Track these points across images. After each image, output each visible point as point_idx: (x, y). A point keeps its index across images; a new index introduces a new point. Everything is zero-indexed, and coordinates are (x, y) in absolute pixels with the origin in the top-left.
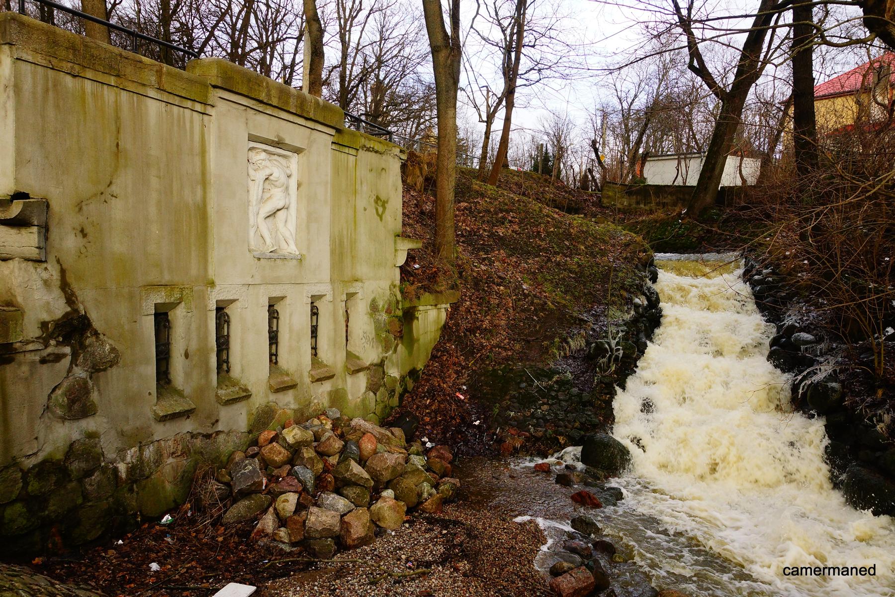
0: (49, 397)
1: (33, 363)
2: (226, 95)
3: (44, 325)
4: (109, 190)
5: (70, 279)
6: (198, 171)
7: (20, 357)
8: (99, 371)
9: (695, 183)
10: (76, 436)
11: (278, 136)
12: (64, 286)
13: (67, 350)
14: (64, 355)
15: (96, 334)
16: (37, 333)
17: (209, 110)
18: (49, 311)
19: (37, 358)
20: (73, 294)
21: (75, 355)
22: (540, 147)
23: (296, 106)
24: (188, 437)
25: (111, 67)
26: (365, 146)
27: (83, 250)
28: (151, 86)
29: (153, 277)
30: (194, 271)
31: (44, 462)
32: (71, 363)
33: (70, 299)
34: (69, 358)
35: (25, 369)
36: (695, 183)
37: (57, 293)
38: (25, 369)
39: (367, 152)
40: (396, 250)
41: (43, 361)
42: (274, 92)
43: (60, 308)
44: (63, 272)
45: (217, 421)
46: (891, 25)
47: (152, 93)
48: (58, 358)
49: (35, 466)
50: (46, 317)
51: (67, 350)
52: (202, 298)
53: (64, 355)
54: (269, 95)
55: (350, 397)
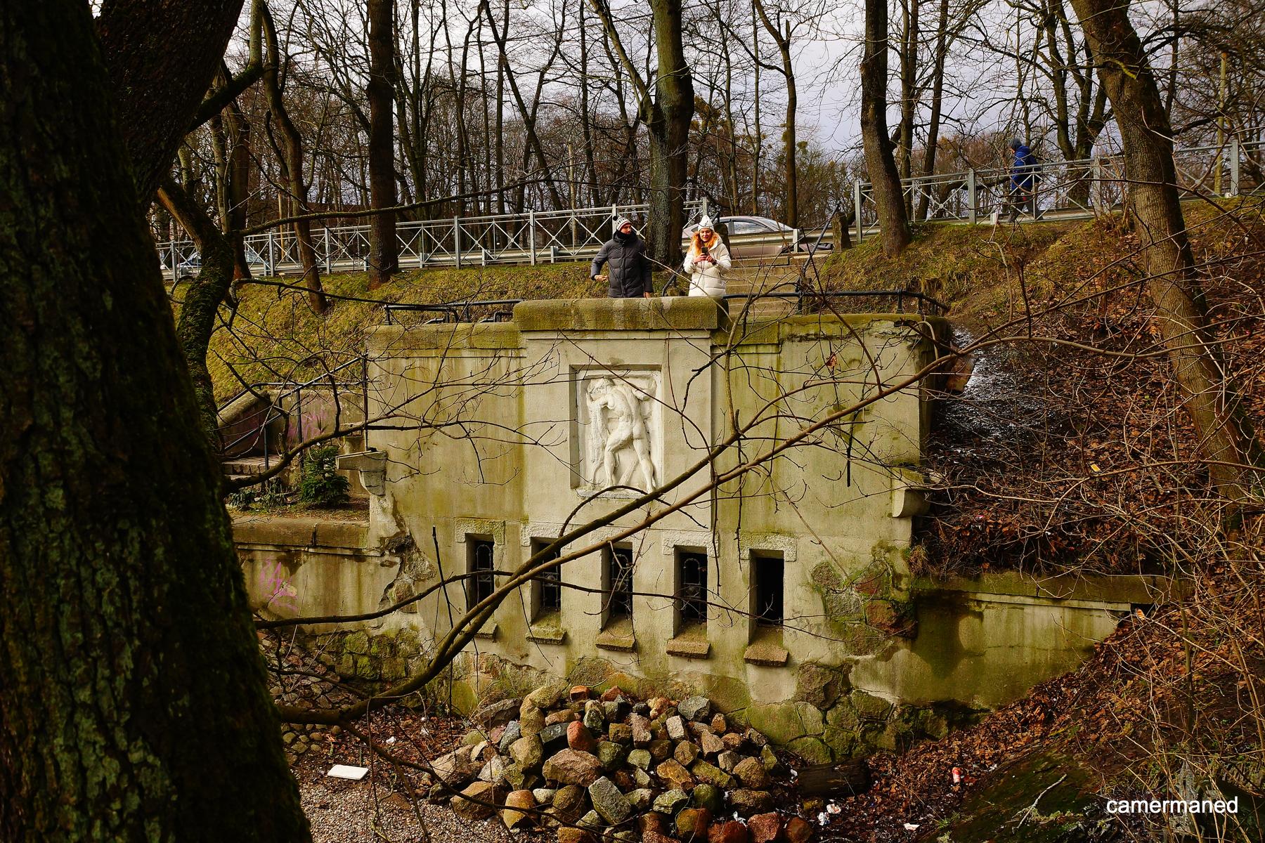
0: (386, 591)
1: (376, 564)
2: (532, 336)
3: (382, 539)
4: (430, 440)
5: (401, 508)
6: (515, 412)
7: (369, 560)
8: (420, 580)
9: (99, 15)
10: (404, 625)
11: (612, 359)
12: (395, 513)
13: (398, 560)
14: (395, 563)
15: (419, 551)
16: (377, 544)
17: (523, 353)
18: (386, 531)
19: (379, 562)
20: (402, 519)
21: (403, 563)
22: (909, 348)
23: (624, 321)
24: (497, 660)
25: (431, 343)
26: (795, 336)
27: (411, 487)
28: (464, 348)
29: (467, 510)
30: (508, 507)
31: (383, 636)
32: (400, 569)
33: (400, 523)
34: (399, 566)
35: (372, 567)
36: (99, 15)
37: (390, 517)
38: (372, 567)
39: (803, 343)
40: (892, 490)
41: (382, 565)
42: (586, 317)
43: (393, 529)
44: (395, 503)
45: (527, 655)
46: (635, 541)
47: (465, 353)
48: (392, 564)
49: (377, 636)
50: (383, 534)
51: (398, 560)
52: (516, 532)
53: (395, 563)
54: (581, 321)
55: (753, 696)
